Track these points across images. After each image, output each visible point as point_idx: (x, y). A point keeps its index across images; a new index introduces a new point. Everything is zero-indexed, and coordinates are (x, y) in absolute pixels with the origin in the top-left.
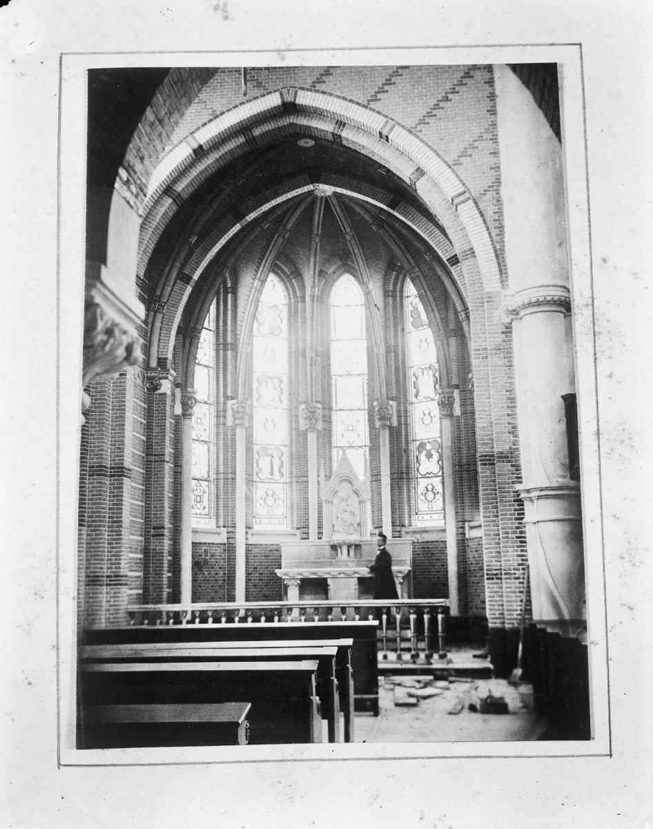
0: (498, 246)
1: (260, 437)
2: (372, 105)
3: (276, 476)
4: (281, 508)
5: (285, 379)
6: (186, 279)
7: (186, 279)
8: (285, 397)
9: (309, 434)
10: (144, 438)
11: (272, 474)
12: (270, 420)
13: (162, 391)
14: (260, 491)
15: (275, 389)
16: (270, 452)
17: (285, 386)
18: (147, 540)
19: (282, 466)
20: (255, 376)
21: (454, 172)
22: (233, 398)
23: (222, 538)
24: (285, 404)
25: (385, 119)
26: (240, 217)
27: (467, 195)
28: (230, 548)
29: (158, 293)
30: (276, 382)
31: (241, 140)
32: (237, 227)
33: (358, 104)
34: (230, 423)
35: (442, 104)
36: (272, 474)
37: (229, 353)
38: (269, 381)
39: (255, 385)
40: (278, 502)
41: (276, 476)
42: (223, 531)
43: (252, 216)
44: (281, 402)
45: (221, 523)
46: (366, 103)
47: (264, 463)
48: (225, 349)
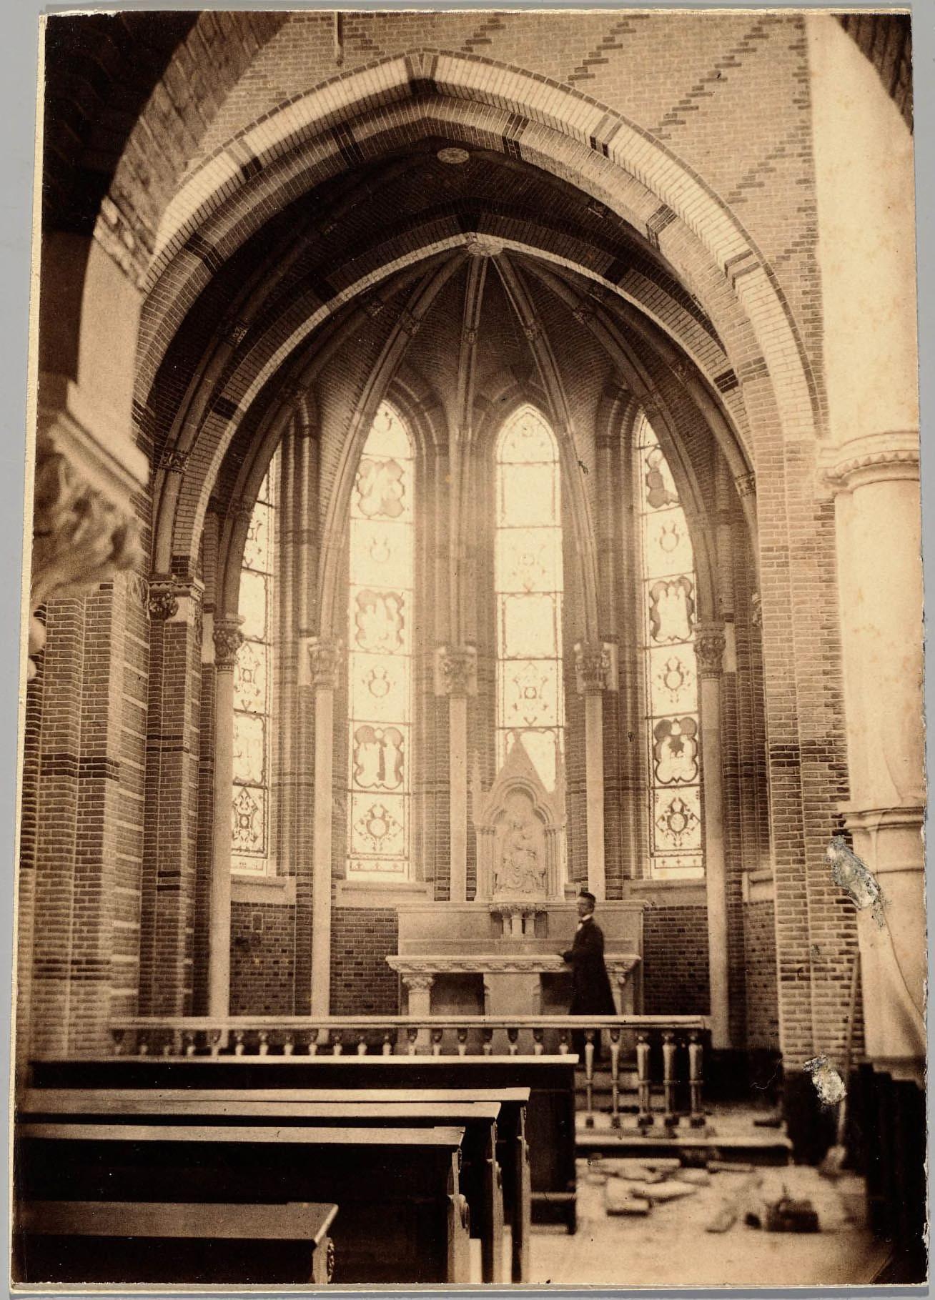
0: (810, 356)
1: (361, 706)
2: (579, 86)
3: (390, 780)
4: (398, 843)
5: (409, 599)
6: (227, 410)
7: (227, 410)
8: (408, 633)
9: (452, 703)
10: (144, 706)
11: (382, 776)
12: (379, 675)
13: (178, 618)
14: (359, 807)
15: (390, 618)
16: (378, 734)
17: (408, 613)
18: (147, 897)
19: (400, 762)
20: (353, 592)
21: (731, 216)
22: (310, 633)
23: (288, 895)
24: (408, 647)
25: (602, 114)
26: (327, 294)
27: (754, 259)
28: (301, 913)
29: (173, 434)
30: (392, 603)
31: (332, 148)
32: (322, 313)
33: (551, 83)
34: (304, 680)
35: (708, 87)
36: (382, 776)
37: (305, 547)
38: (380, 602)
39: (353, 608)
40: (392, 830)
41: (390, 780)
42: (290, 881)
43: (347, 294)
44: (401, 641)
45: (286, 867)
46: (566, 82)
47: (368, 757)
48: (298, 543)
